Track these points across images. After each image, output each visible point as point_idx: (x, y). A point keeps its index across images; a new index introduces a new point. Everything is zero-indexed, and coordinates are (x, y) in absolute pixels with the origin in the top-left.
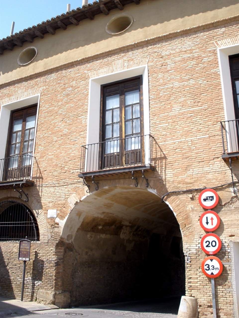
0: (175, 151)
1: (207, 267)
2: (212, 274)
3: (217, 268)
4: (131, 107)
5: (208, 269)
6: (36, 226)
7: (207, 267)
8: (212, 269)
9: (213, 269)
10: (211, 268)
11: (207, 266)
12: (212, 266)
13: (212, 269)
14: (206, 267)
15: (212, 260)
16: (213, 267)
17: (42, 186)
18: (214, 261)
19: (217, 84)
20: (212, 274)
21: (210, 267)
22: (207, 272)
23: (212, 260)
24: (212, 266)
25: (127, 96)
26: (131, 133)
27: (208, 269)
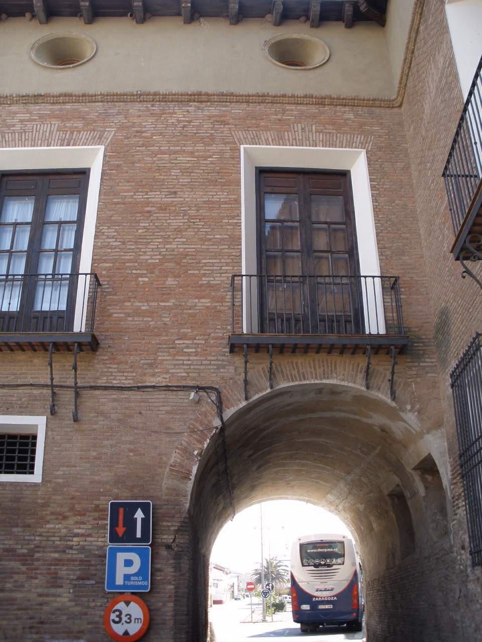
0: (174, 508)
1: (117, 616)
2: (126, 633)
3: (138, 619)
4: (11, 229)
5: (117, 619)
6: (20, 439)
7: (117, 616)
8: (126, 622)
9: (128, 621)
10: (124, 619)
11: (117, 613)
12: (126, 616)
13: (126, 622)
14: (113, 616)
15: (127, 603)
16: (128, 616)
17: (283, 114)
18: (132, 604)
19: (464, 163)
20: (126, 633)
21: (123, 616)
22: (114, 626)
23: (127, 603)
24: (126, 616)
25: (238, 512)
26: (54, 248)
27: (117, 619)
